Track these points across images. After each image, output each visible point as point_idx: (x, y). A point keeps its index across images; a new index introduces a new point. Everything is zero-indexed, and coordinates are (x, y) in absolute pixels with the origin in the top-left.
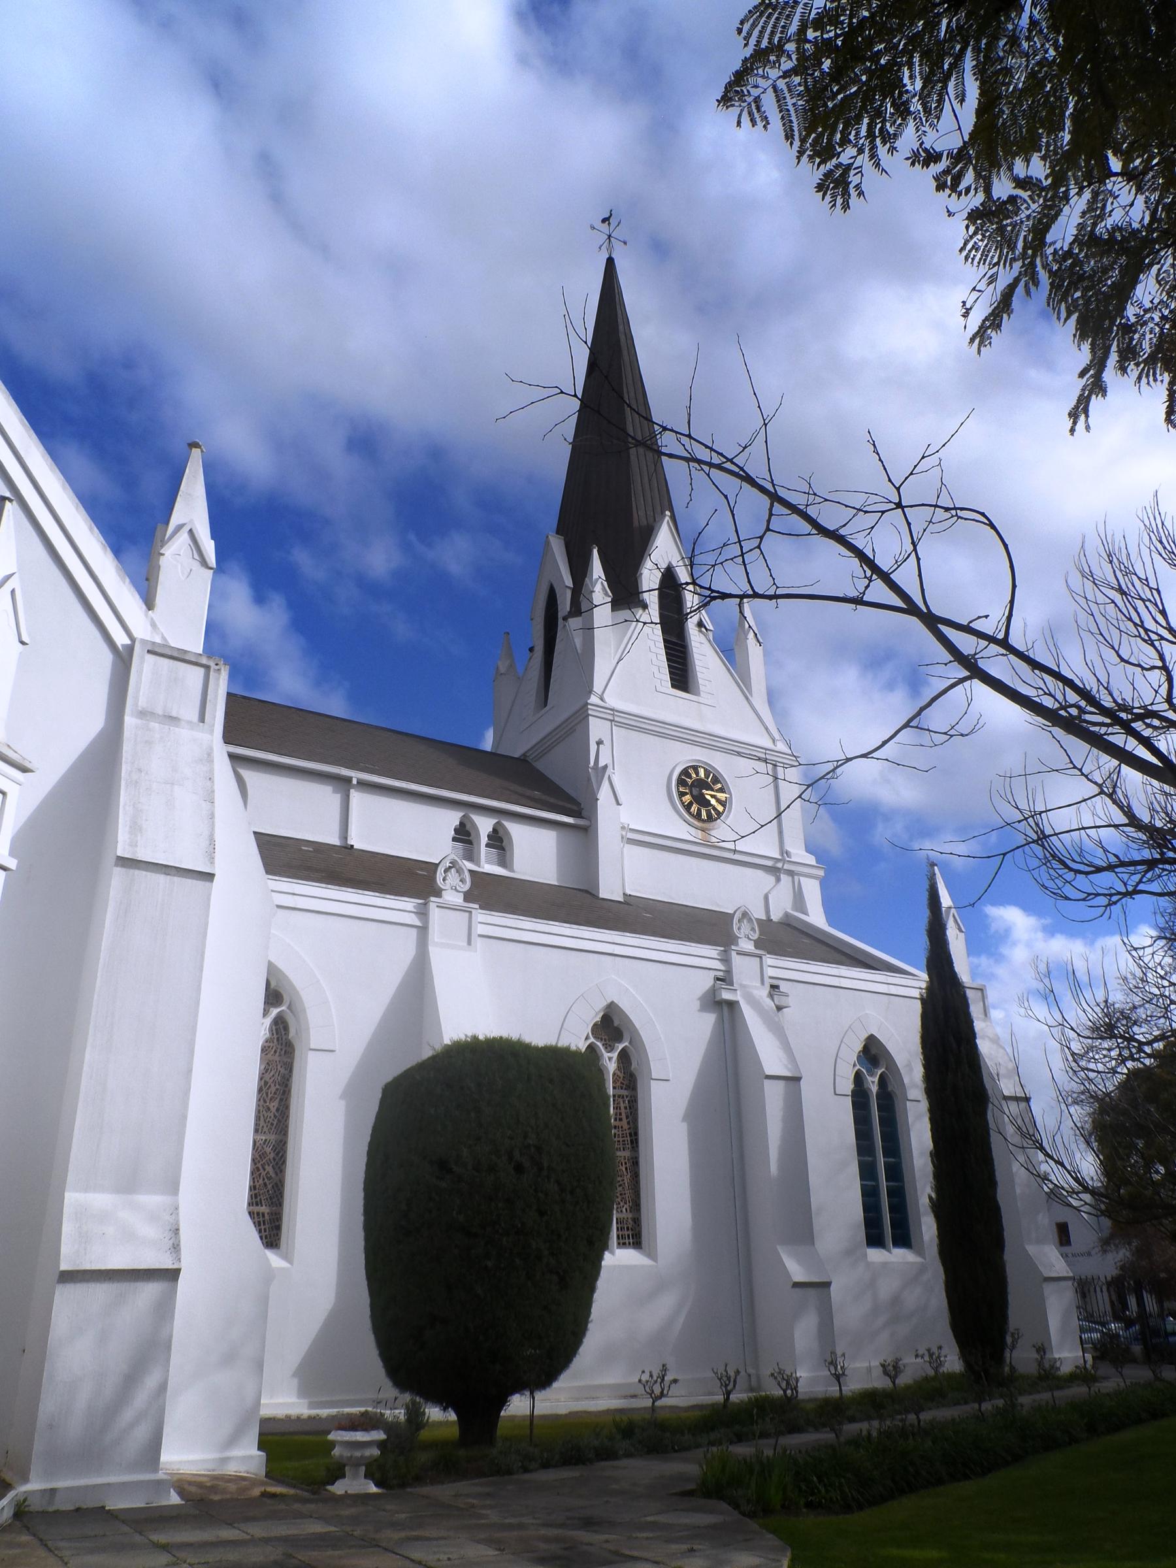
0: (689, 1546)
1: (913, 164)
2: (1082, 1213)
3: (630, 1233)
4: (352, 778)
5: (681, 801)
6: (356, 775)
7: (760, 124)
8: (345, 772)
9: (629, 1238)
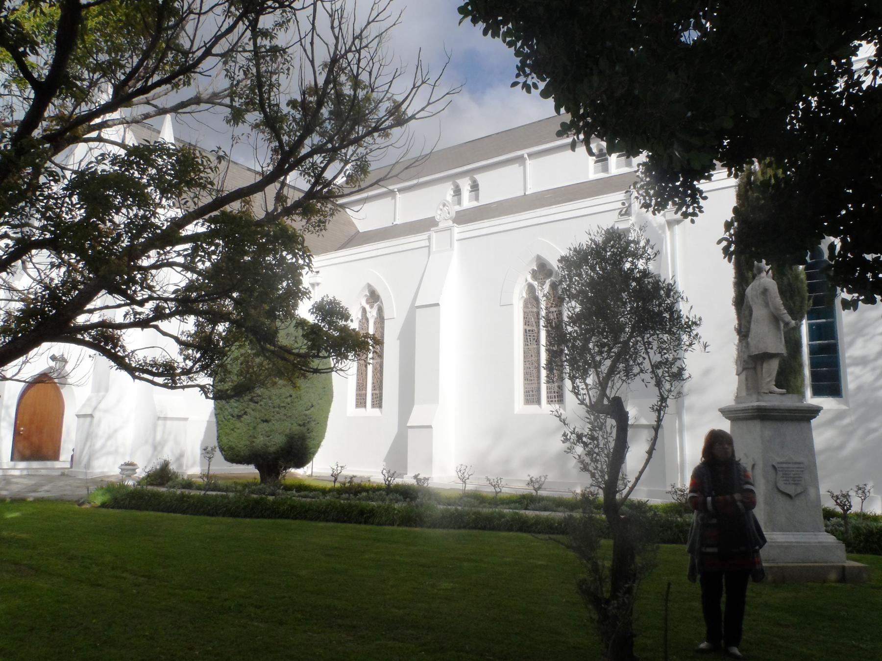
0: (83, 507)
1: (237, 116)
2: (401, 161)
3: (556, 394)
4: (523, 154)
5: (430, 243)
6: (525, 152)
7: (801, 479)
8: (519, 153)
9: (555, 398)
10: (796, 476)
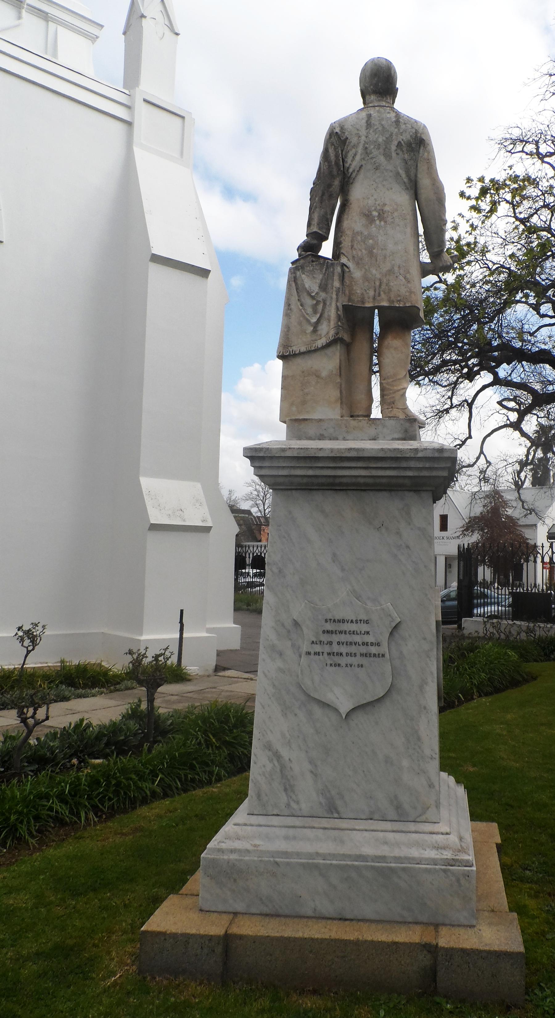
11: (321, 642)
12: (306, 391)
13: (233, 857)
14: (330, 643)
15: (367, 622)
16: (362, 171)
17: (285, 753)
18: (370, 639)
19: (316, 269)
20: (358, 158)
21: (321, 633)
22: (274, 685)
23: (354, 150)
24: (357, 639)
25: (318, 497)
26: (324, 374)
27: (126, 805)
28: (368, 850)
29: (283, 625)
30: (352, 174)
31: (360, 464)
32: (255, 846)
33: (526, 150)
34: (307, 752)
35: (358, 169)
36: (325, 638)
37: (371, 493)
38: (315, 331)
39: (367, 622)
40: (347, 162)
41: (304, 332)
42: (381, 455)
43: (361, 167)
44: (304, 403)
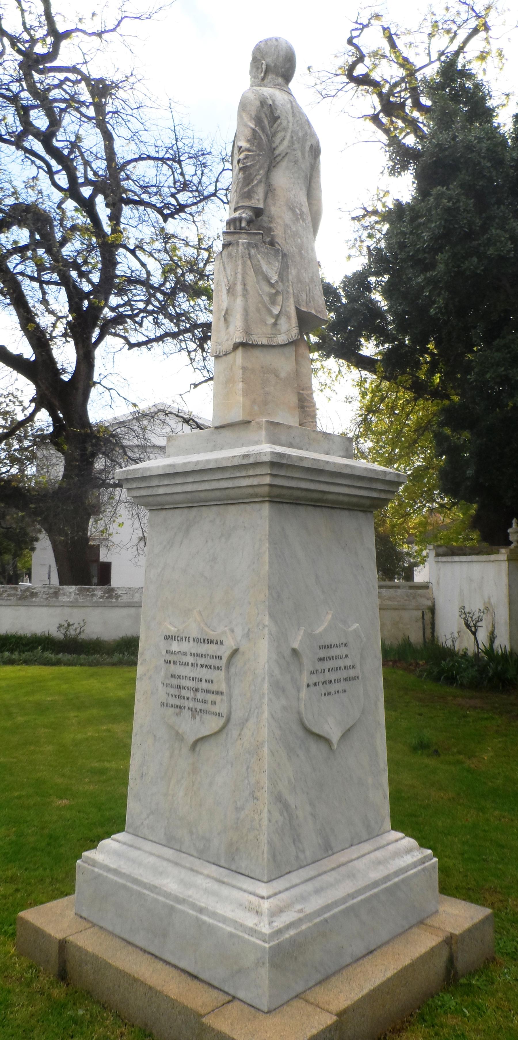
10: (204, 685)
11: (317, 671)
12: (267, 389)
13: (292, 932)
14: (323, 671)
15: (346, 645)
16: (286, 159)
17: (291, 800)
18: (348, 662)
19: (270, 253)
20: (286, 143)
21: (317, 661)
22: (280, 727)
23: (283, 133)
24: (341, 663)
25: (302, 511)
26: (283, 375)
27: (209, 917)
28: (375, 875)
29: (284, 657)
30: (277, 156)
31: (347, 482)
32: (300, 911)
33: (33, 113)
34: (308, 794)
35: (284, 154)
36: (319, 666)
37: (338, 511)
38: (275, 324)
39: (346, 645)
40: (274, 142)
41: (264, 322)
42: (365, 474)
43: (287, 154)
44: (265, 403)
